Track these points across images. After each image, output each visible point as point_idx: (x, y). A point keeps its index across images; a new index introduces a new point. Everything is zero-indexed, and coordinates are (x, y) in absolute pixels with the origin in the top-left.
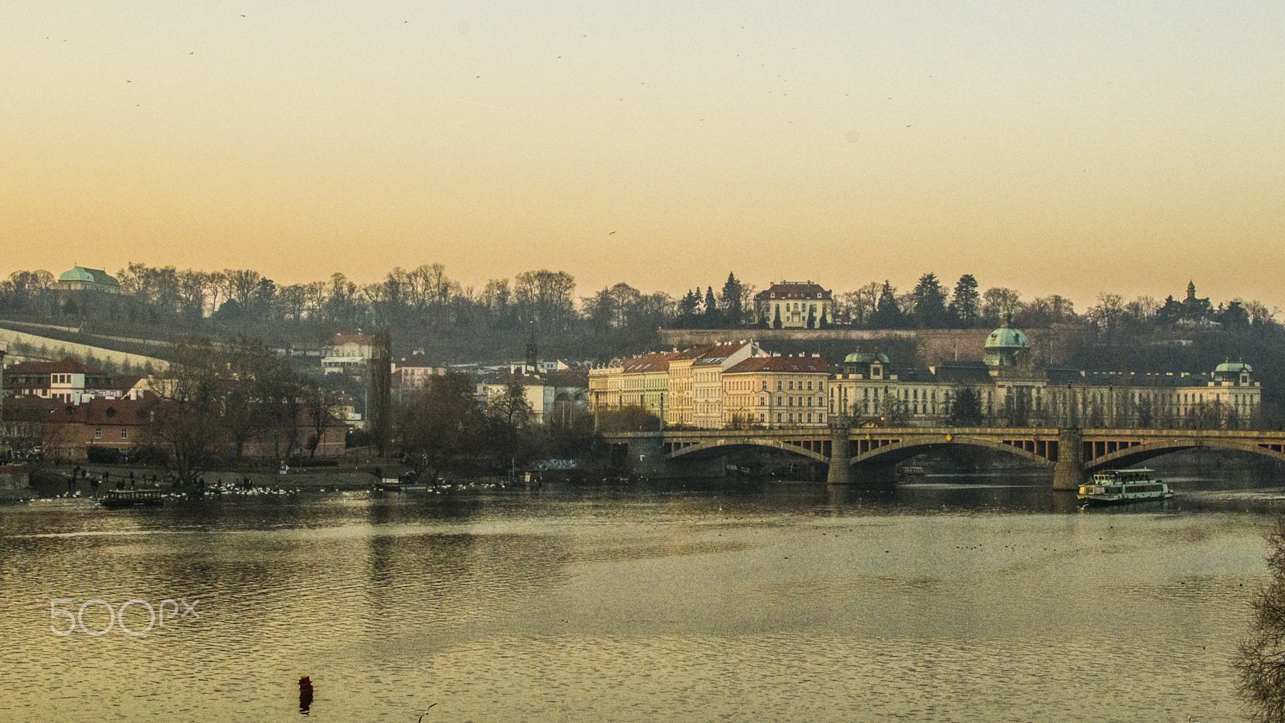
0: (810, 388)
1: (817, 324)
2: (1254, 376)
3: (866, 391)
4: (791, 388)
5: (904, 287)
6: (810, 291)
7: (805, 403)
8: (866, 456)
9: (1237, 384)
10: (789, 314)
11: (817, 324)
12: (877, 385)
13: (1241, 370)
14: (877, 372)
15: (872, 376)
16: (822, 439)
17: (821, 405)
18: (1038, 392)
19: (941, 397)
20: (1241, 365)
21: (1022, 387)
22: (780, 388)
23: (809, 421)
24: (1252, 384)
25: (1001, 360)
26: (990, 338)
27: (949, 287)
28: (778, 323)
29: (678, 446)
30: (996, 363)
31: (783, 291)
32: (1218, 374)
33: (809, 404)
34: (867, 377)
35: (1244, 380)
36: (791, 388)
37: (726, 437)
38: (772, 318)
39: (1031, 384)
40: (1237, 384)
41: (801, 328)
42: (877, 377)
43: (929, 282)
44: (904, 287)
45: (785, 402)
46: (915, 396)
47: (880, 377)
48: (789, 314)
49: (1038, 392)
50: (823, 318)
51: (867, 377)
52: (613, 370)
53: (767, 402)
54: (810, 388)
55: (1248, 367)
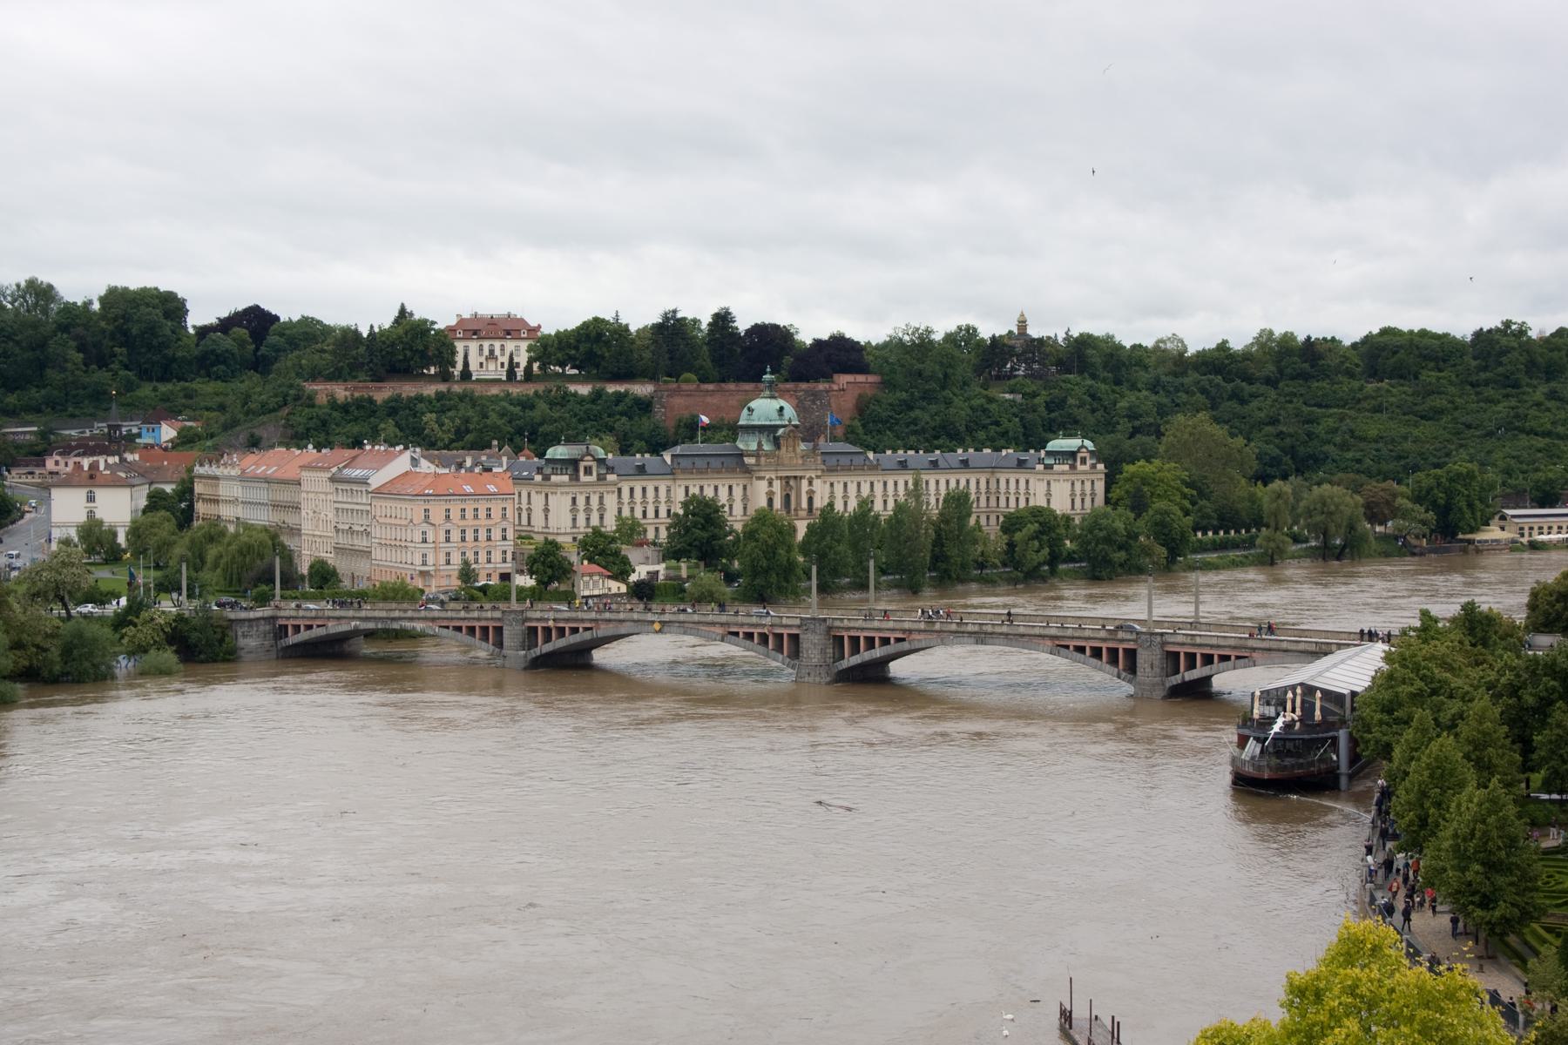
0: (489, 516)
1: (520, 373)
2: (1097, 455)
3: (574, 500)
4: (463, 517)
6: (508, 328)
7: (482, 535)
8: (548, 648)
9: (1073, 467)
11: (520, 373)
12: (1083, 477)
14: (588, 471)
16: (491, 624)
17: (504, 538)
18: (810, 483)
19: (680, 496)
21: (788, 477)
22: (448, 517)
23: (489, 561)
24: (1093, 466)
25: (760, 445)
26: (745, 411)
28: (466, 375)
29: (297, 629)
30: (754, 446)
32: (1049, 454)
33: (489, 539)
34: (575, 477)
35: (1084, 461)
36: (463, 517)
37: (360, 619)
38: (460, 366)
39: (798, 474)
40: (1073, 467)
41: (498, 381)
45: (455, 536)
47: (593, 478)
48: (483, 359)
49: (810, 483)
50: (528, 369)
51: (575, 477)
52: (226, 472)
53: (430, 538)
54: (489, 516)
55: (1088, 443)
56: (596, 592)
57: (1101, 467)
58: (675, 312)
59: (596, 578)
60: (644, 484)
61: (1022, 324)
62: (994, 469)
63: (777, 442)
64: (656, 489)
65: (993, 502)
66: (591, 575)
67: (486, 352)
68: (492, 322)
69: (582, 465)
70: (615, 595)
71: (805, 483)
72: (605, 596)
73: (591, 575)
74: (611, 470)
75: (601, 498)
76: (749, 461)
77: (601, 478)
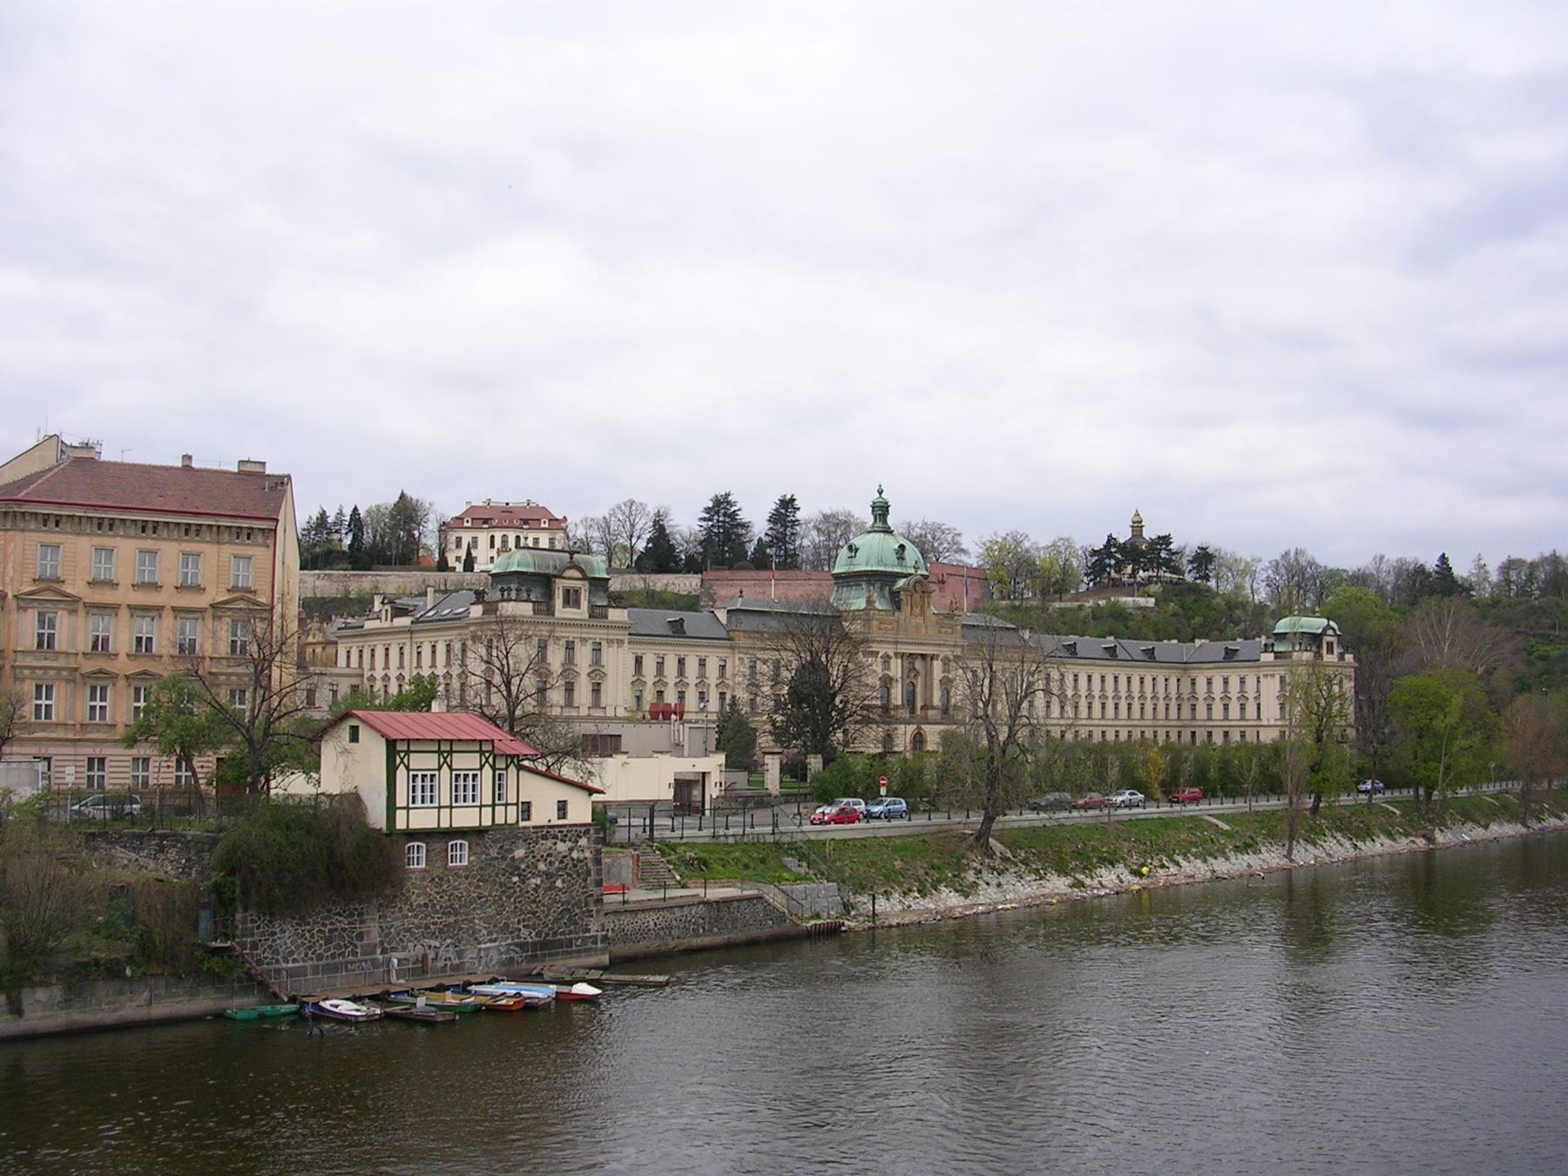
5: (687, 524)
6: (529, 518)
9: (1318, 655)
10: (494, 553)
12: (572, 634)
13: (1324, 633)
14: (571, 598)
15: (561, 611)
18: (946, 670)
20: (1324, 622)
24: (1341, 657)
25: (869, 602)
27: (757, 518)
30: (860, 603)
31: (482, 518)
42: (570, 613)
43: (721, 507)
44: (687, 524)
46: (681, 672)
47: (582, 612)
48: (494, 553)
51: (545, 606)
56: (466, 818)
57: (1349, 657)
58: (728, 495)
59: (466, 761)
60: (682, 652)
61: (1137, 526)
62: (1185, 665)
63: (895, 600)
64: (702, 663)
65: (1186, 712)
66: (446, 748)
67: (498, 544)
68: (507, 510)
69: (560, 585)
70: (546, 832)
71: (937, 665)
72: (507, 834)
73: (446, 748)
74: (618, 600)
75: (597, 650)
76: (855, 628)
77: (596, 613)
